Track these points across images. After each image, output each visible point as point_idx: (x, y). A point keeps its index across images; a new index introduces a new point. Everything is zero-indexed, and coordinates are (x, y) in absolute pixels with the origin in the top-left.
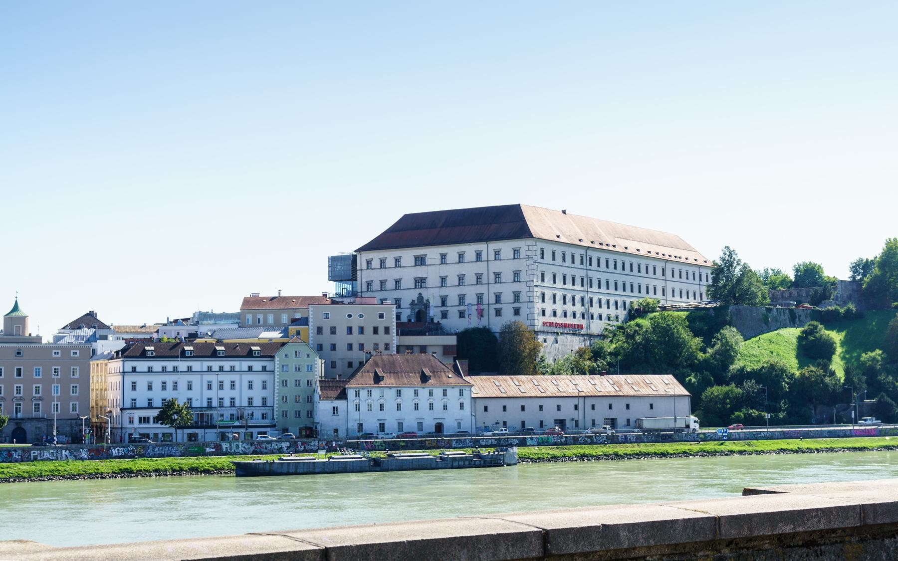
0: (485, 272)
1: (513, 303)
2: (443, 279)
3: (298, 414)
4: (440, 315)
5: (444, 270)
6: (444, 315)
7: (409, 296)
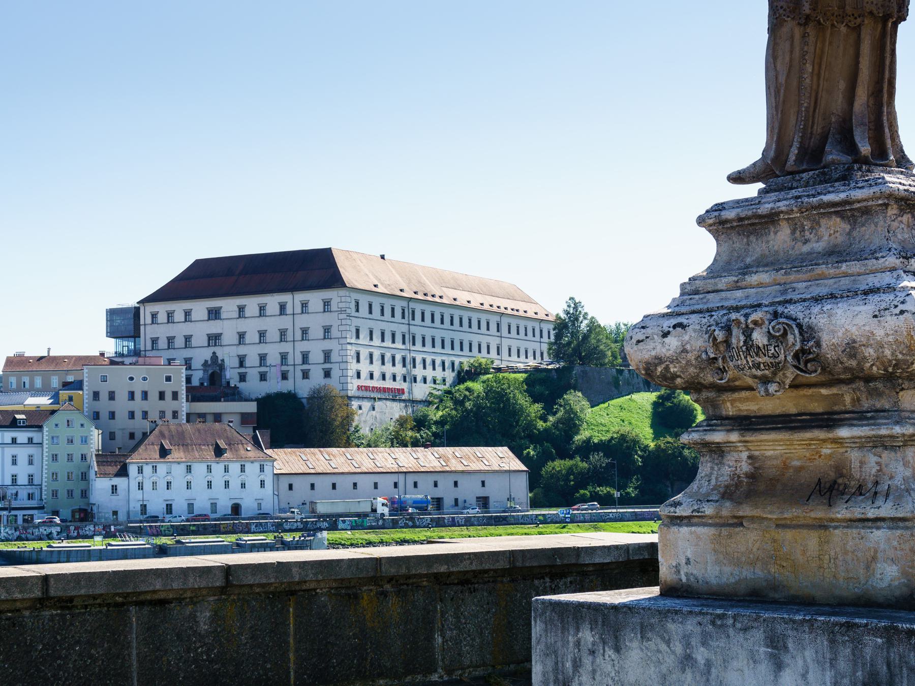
0: (291, 351)
1: (323, 363)
2: (242, 336)
3: (70, 493)
4: (237, 378)
5: (242, 325)
6: (243, 378)
7: (201, 355)
